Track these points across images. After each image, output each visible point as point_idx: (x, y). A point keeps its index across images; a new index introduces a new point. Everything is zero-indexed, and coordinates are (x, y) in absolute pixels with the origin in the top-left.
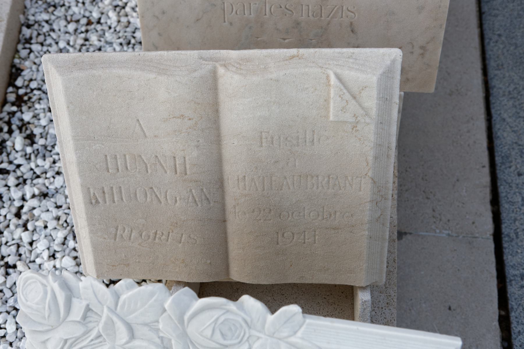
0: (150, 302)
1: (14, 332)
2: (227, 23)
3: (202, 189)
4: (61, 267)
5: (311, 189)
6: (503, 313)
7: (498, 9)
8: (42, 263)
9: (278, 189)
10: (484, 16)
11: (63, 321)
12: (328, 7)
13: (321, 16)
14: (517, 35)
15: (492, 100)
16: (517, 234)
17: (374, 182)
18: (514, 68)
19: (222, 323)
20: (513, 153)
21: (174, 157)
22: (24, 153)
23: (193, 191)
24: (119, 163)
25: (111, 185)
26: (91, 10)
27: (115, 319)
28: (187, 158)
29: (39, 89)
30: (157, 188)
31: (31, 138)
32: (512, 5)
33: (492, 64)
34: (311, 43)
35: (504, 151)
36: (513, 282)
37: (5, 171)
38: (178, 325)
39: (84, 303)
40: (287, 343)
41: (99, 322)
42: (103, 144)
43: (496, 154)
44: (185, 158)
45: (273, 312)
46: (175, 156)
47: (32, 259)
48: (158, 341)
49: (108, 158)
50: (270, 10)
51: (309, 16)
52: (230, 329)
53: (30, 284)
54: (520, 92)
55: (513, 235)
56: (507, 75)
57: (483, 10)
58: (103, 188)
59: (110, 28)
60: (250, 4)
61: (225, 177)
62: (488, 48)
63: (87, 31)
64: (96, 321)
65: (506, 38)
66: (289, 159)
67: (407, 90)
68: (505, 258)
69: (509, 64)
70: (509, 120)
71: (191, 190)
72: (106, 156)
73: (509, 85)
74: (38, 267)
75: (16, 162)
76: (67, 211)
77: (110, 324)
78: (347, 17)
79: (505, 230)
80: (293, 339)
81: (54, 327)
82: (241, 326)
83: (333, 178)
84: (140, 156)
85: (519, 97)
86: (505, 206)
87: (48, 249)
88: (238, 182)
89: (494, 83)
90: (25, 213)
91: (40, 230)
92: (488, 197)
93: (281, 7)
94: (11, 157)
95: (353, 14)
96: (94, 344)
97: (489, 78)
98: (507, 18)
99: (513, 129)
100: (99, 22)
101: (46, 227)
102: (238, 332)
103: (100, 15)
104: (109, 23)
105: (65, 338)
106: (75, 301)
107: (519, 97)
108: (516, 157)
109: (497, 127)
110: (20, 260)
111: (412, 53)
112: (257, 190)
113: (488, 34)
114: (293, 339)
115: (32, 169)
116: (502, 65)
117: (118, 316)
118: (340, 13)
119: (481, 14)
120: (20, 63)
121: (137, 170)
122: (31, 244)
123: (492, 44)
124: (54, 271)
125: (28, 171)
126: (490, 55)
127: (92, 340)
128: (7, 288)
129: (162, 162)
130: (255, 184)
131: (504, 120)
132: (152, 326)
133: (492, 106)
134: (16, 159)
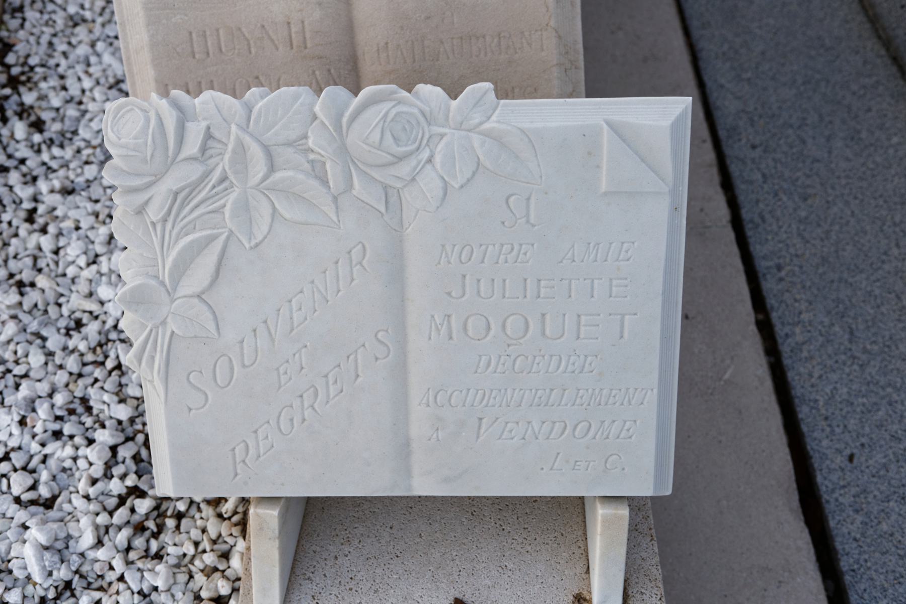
0: (295, 107)
1: (41, 367)
3: (329, 70)
4: (110, 270)
5: (477, 56)
6: (761, 317)
8: (77, 275)
9: (433, 60)
11: (172, 163)
15: (702, 64)
16: (763, 220)
17: (559, 37)
19: (392, 120)
21: (289, 23)
22: (29, 144)
23: (317, 73)
24: (209, 44)
25: (199, 79)
27: (247, 140)
28: (306, 23)
29: (43, 66)
30: (266, 76)
31: (38, 126)
33: (694, 24)
36: (768, 276)
37: (2, 169)
38: (334, 133)
39: (204, 124)
40: (480, 133)
41: (224, 154)
42: (186, 15)
44: (303, 22)
45: (454, 97)
46: (290, 21)
47: (60, 271)
48: (307, 166)
49: (194, 35)
52: (404, 129)
53: (122, 116)
55: (757, 220)
58: (187, 84)
61: (360, 53)
64: (221, 154)
66: (444, 14)
68: (752, 248)
71: (314, 72)
72: (191, 33)
74: (70, 281)
75: (18, 155)
76: (108, 203)
77: (241, 147)
79: (746, 214)
80: (487, 126)
81: (158, 177)
82: (418, 123)
83: (504, 37)
84: (239, 29)
86: (741, 188)
87: (85, 253)
88: (379, 54)
90: (41, 216)
91: (70, 232)
92: (716, 178)
94: (10, 150)
96: (217, 194)
101: (78, 228)
102: (414, 132)
105: (174, 188)
106: (190, 125)
110: (63, 204)
112: (405, 62)
114: (487, 126)
115: (44, 164)
117: (251, 135)
120: (9, 37)
121: (236, 51)
122: (56, 252)
124: (99, 278)
125: (38, 167)
127: (214, 187)
128: (24, 312)
129: (270, 33)
130: (402, 54)
131: (722, 86)
132: (298, 143)
133: (703, 72)
134: (17, 150)
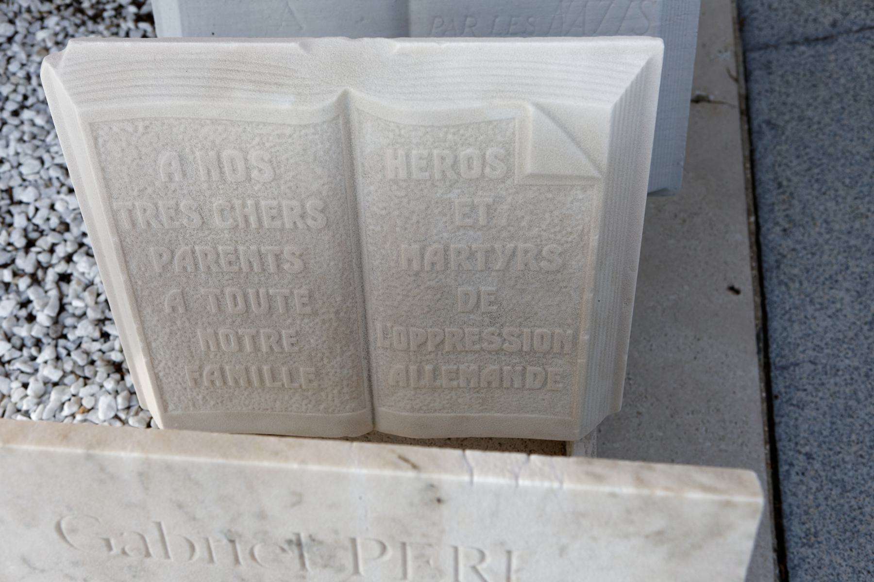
10: (777, 403)
18: (841, 546)
32: (832, 381)
57: (775, 390)
62: (787, 487)
65: (823, 464)
97: (790, 565)
98: (824, 414)
116: (816, 535)
119: (770, 398)
123: (795, 478)
126: (790, 505)
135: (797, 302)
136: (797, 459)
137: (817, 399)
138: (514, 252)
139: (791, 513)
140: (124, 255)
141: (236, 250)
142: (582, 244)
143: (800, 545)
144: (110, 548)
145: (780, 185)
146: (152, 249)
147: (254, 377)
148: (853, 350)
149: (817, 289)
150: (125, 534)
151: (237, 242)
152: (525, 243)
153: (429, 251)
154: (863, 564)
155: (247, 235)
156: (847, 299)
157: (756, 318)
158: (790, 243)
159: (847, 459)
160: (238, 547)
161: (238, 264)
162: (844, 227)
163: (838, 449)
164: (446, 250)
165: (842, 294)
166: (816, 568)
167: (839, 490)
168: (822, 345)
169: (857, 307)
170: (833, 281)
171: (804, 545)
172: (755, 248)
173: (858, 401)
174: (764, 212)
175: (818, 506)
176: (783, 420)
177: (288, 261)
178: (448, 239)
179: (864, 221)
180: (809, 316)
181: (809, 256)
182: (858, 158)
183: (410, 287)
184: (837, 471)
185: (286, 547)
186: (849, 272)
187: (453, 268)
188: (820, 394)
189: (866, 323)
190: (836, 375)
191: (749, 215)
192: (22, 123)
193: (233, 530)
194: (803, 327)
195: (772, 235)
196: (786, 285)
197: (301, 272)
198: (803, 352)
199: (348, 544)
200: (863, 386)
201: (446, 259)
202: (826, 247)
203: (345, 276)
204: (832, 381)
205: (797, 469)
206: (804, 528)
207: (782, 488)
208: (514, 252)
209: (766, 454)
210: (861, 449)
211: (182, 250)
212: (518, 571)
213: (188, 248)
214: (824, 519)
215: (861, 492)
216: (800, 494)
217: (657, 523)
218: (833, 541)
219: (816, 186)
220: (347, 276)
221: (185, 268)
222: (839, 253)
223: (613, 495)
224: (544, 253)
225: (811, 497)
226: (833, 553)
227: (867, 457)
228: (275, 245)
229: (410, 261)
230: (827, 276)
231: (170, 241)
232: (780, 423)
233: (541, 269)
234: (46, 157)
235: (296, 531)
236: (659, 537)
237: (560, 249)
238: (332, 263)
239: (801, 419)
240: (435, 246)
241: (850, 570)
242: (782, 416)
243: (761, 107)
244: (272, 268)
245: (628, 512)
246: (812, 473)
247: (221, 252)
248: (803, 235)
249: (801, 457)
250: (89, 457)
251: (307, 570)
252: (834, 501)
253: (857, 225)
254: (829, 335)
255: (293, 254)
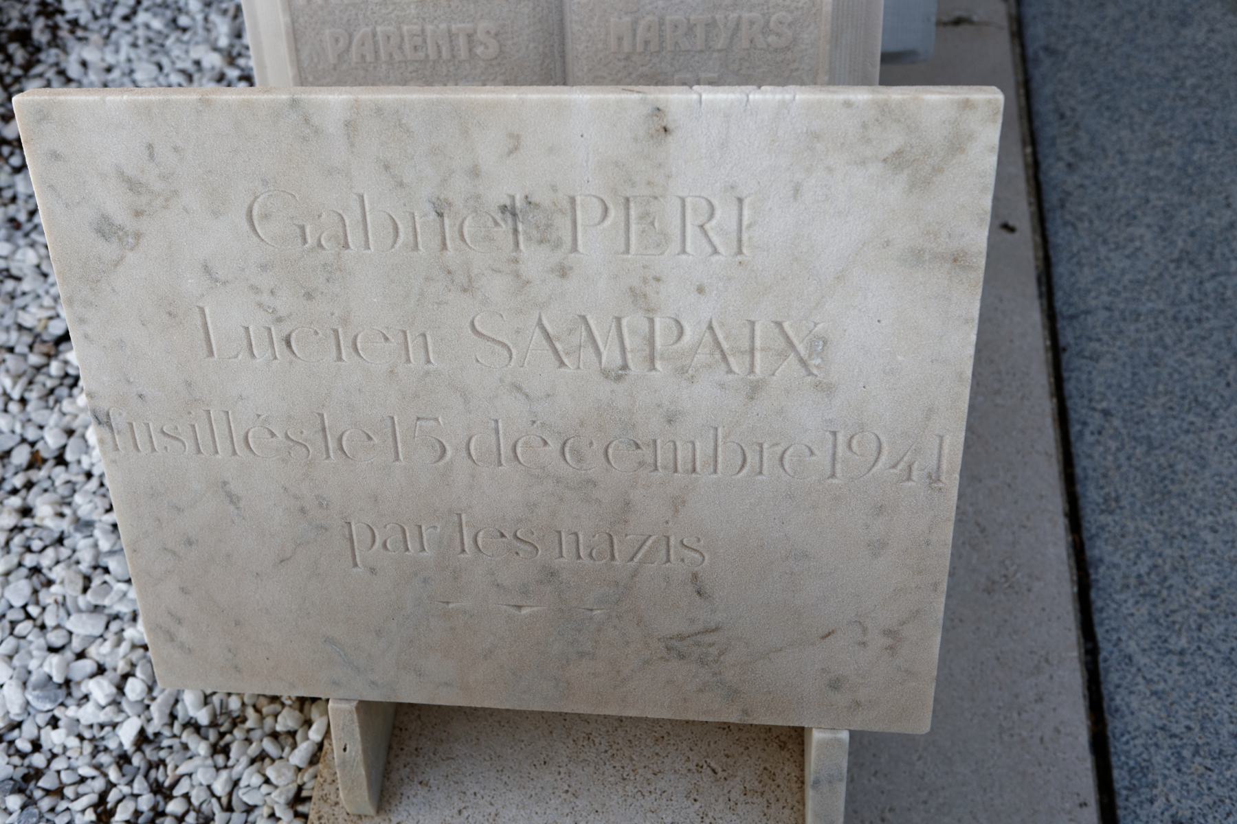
2: (360, 569)
7: (1099, 340)
10: (1065, 357)
12: (628, 537)
13: (613, 557)
14: (1149, 414)
18: (1148, 510)
20: (1158, 759)
26: (42, 423)
32: (1132, 328)
33: (1091, 495)
34: (591, 618)
35: (1134, 752)
43: (1114, 759)
50: (475, 541)
51: (579, 557)
54: (1165, 579)
56: (1131, 526)
57: (1063, 341)
59: (89, 475)
60: (420, 527)
62: (1079, 448)
63: (29, 485)
65: (1124, 420)
67: (856, 727)
69: (1133, 495)
70: (1142, 660)
73: (1138, 556)
78: (683, 560)
85: (1165, 593)
89: (1098, 549)
93: (503, 535)
95: (697, 556)
97: (1085, 535)
98: (1124, 364)
99: (1154, 687)
100: (60, 460)
103: (63, 441)
104: (85, 465)
107: (1165, 593)
108: (1166, 772)
109: (1112, 679)
111: (864, 644)
113: (1077, 409)
116: (1117, 499)
118: (664, 552)
119: (1056, 350)
123: (1089, 438)
126: (1084, 469)
133: (1096, 618)
135: (1087, 243)
136: (1092, 417)
137: (1115, 349)
138: (738, 25)
139: (1086, 478)
140: (296, 40)
141: (423, 31)
142: (814, 10)
143: (1097, 512)
144: (305, 241)
145: (1062, 116)
146: (327, 32)
147: (458, 96)
148: (1157, 292)
149: (1111, 228)
150: (324, 216)
151: (424, 19)
152: (751, 11)
153: (643, 24)
154: (1176, 528)
155: (436, 11)
156: (1148, 236)
157: (1036, 258)
158: (1076, 179)
159: (1153, 412)
160: (447, 221)
161: (424, 49)
162: (1143, 157)
163: (1141, 402)
164: (661, 23)
165: (1142, 230)
166: (1118, 537)
167: (1144, 448)
168: (1119, 288)
169: (1161, 243)
170: (1131, 217)
171: (1102, 512)
172: (1032, 182)
173: (1165, 348)
174: (1043, 148)
175: (1119, 467)
176: (1074, 375)
177: (481, 43)
178: (663, 9)
179: (1166, 149)
180: (1102, 257)
181: (1101, 192)
182: (1157, 80)
183: (620, 75)
184: (1142, 426)
185: (498, 217)
186: (1150, 205)
187: (669, 49)
188: (1118, 343)
189: (1172, 261)
190: (1137, 320)
191: (1024, 145)
192: (135, 28)
193: (442, 197)
194: (1095, 270)
195: (1054, 171)
196: (1074, 226)
197: (496, 58)
198: (1096, 298)
199: (566, 205)
200: (1170, 331)
201: (661, 36)
202: (1121, 181)
203: (545, 64)
204: (1132, 328)
205: (1091, 427)
206: (1103, 492)
207: (1073, 450)
208: (738, 25)
209: (1053, 409)
210: (1171, 400)
211: (362, 31)
212: (749, 226)
213: (369, 29)
214: (1127, 481)
215: (1172, 449)
216: (1096, 455)
217: (895, 140)
218: (1138, 505)
219: (1107, 114)
220: (548, 65)
221: (363, 57)
222: (1137, 186)
223: (848, 104)
224: (772, 25)
225: (1110, 458)
226: (1139, 519)
227: (1178, 408)
228: (468, 22)
229: (620, 39)
230: (1122, 211)
231: (349, 20)
232: (1070, 378)
233: (769, 45)
234: (165, 61)
235: (511, 192)
236: (897, 161)
237: (790, 18)
238: (532, 46)
239: (1095, 373)
240: (650, 18)
241: (1160, 536)
242: (1072, 371)
243: (1037, 32)
244: (463, 54)
245: (865, 126)
246: (1111, 431)
247: (406, 34)
248: (1092, 169)
249: (1097, 415)
250: (294, 103)
251: (521, 251)
252: (1138, 460)
253: (1158, 154)
254: (1127, 277)
255: (488, 32)
